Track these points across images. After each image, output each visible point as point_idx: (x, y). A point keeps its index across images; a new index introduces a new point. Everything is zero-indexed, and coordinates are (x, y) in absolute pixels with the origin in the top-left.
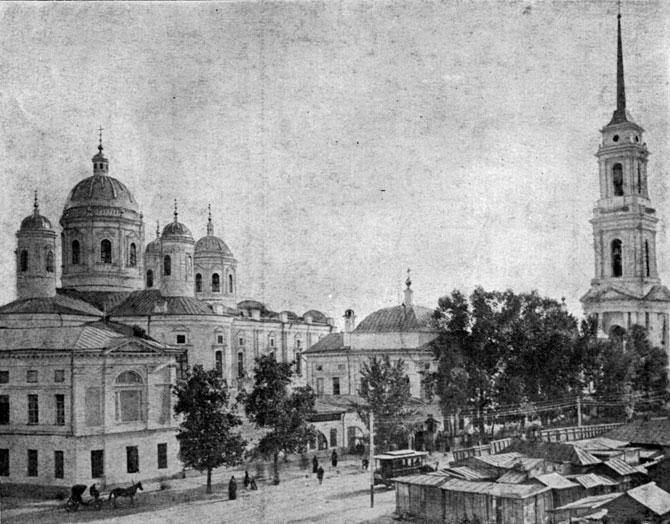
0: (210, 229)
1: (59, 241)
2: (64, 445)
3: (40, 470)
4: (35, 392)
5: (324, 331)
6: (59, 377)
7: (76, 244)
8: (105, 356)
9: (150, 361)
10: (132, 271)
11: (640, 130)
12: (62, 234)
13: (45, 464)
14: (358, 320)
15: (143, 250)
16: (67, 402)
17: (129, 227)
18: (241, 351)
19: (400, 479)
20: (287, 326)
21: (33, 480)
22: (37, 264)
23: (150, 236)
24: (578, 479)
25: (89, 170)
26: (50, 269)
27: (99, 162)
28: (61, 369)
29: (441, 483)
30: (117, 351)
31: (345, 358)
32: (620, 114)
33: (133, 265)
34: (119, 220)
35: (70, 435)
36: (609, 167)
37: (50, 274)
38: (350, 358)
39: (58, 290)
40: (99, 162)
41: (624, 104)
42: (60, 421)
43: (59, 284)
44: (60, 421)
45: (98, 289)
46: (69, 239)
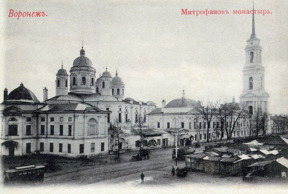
0: (117, 74)
1: (69, 77)
2: (70, 142)
3: (63, 150)
4: (62, 124)
5: (154, 108)
6: (70, 119)
7: (74, 78)
8: (85, 113)
9: (99, 115)
10: (93, 87)
11: (259, 40)
12: (70, 75)
13: (65, 149)
14: (166, 104)
15: (96, 81)
16: (72, 128)
17: (91, 73)
18: (127, 114)
19: (187, 156)
20: (142, 106)
21: (60, 154)
22: (63, 83)
23: (97, 76)
24: (252, 156)
25: (78, 55)
26: (66, 86)
27: (82, 52)
28: (71, 117)
29: (203, 157)
30: (89, 111)
31: (162, 116)
32: (253, 34)
33: (93, 85)
34: (88, 70)
35: (73, 139)
36: (249, 52)
37: (66, 88)
38: (164, 116)
39: (69, 93)
40: (82, 52)
41: (43, 147)
42: (70, 134)
43: (69, 91)
44: (70, 135)
45: (80, 93)
46: (72, 77)
